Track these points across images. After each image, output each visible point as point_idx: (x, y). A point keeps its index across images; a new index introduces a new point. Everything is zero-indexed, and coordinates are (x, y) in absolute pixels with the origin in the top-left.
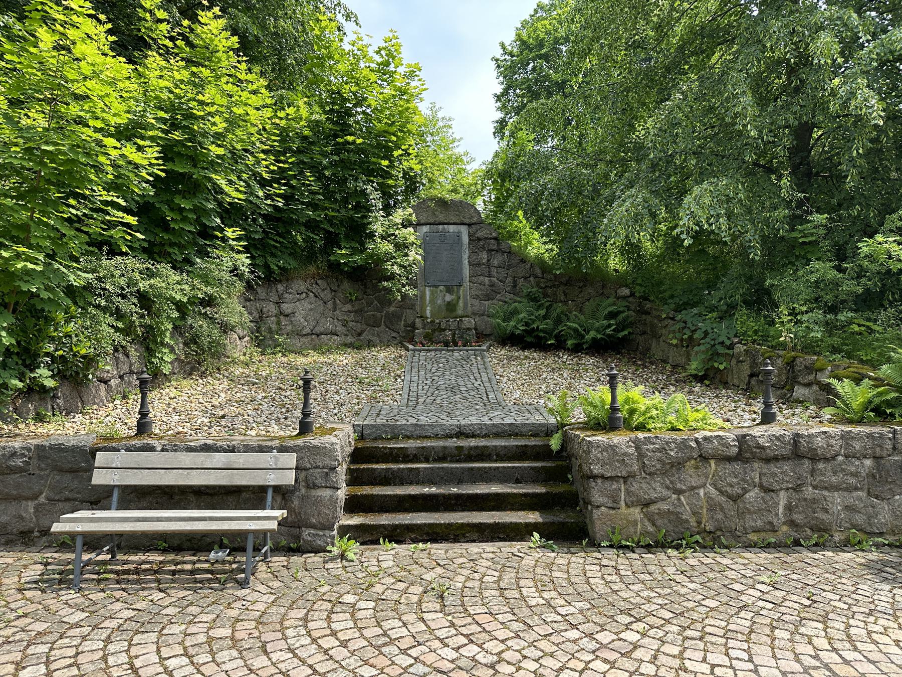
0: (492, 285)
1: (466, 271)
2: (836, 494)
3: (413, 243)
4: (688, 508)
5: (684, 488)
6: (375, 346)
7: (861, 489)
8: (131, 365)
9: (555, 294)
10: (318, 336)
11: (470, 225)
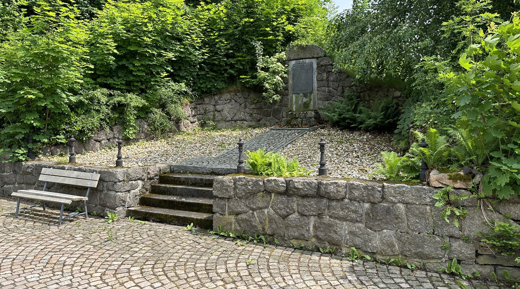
0: (329, 92)
1: (315, 85)
2: (344, 223)
4: (258, 219)
5: (254, 207)
7: (360, 222)
8: (114, 134)
11: (317, 58)
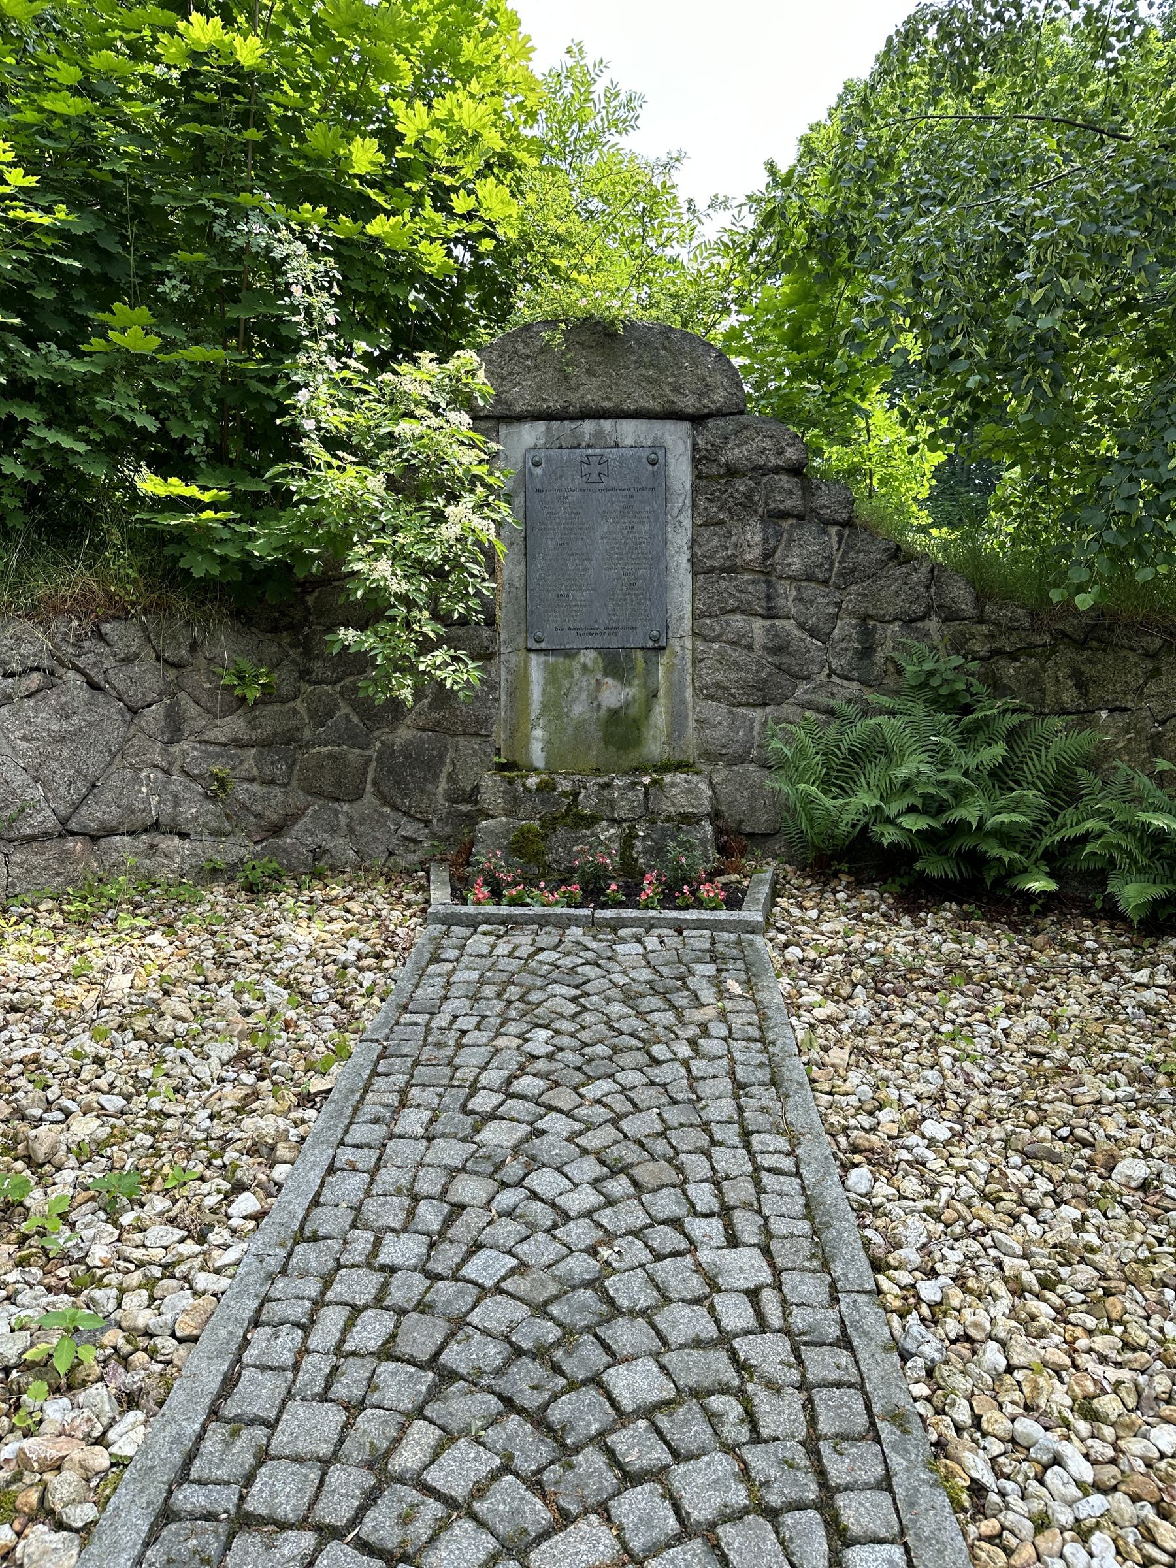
0: (779, 648)
3: (475, 479)
6: (336, 870)
9: (1034, 681)
10: (94, 839)
11: (697, 419)
